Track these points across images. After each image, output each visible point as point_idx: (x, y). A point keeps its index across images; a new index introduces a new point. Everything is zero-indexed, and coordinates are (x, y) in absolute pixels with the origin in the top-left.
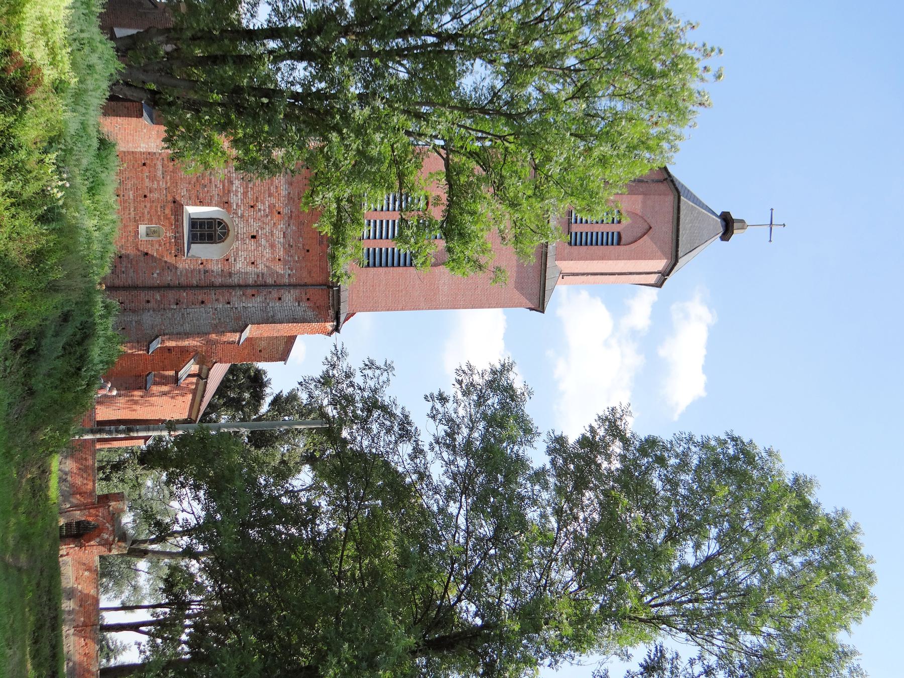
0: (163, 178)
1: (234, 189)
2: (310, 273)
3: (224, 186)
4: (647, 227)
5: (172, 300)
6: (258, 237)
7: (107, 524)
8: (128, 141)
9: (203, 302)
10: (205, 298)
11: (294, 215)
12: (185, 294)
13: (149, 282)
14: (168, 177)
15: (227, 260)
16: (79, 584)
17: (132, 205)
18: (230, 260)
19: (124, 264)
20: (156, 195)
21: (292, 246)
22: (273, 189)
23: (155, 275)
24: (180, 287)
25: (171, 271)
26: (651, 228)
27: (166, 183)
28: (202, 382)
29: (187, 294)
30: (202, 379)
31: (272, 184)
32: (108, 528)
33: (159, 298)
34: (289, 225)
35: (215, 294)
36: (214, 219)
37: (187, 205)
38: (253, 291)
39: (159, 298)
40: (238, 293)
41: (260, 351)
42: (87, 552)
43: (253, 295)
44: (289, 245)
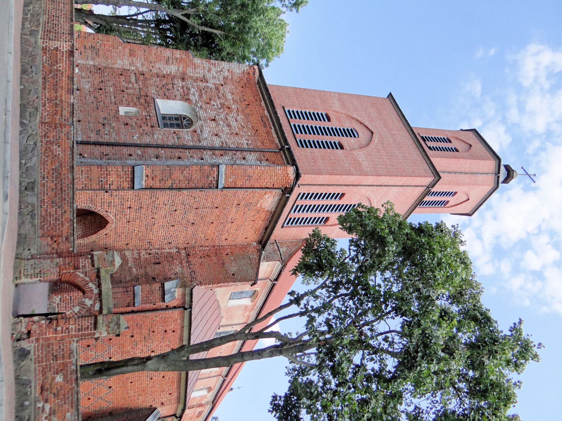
0: (136, 82)
1: (192, 92)
2: (263, 143)
3: (184, 91)
4: (465, 198)
5: (152, 155)
6: (216, 120)
7: (91, 285)
8: (107, 57)
9: (179, 158)
10: (181, 155)
11: (240, 110)
12: (163, 151)
13: (129, 141)
14: (140, 83)
15: (195, 132)
16: (46, 401)
17: (112, 94)
18: (197, 132)
19: (107, 129)
20: (131, 91)
21: (244, 127)
22: (220, 95)
23: (135, 138)
24: (158, 146)
25: (149, 136)
26: (471, 146)
27: (139, 86)
28: (187, 312)
29: (165, 152)
30: (186, 309)
31: (219, 92)
32: (92, 290)
33: (140, 153)
34: (238, 115)
35: (189, 153)
36: (180, 116)
37: (157, 98)
38: (221, 152)
39: (140, 153)
40: (209, 153)
41: (233, 275)
42: (59, 328)
43: (222, 155)
44: (241, 126)
